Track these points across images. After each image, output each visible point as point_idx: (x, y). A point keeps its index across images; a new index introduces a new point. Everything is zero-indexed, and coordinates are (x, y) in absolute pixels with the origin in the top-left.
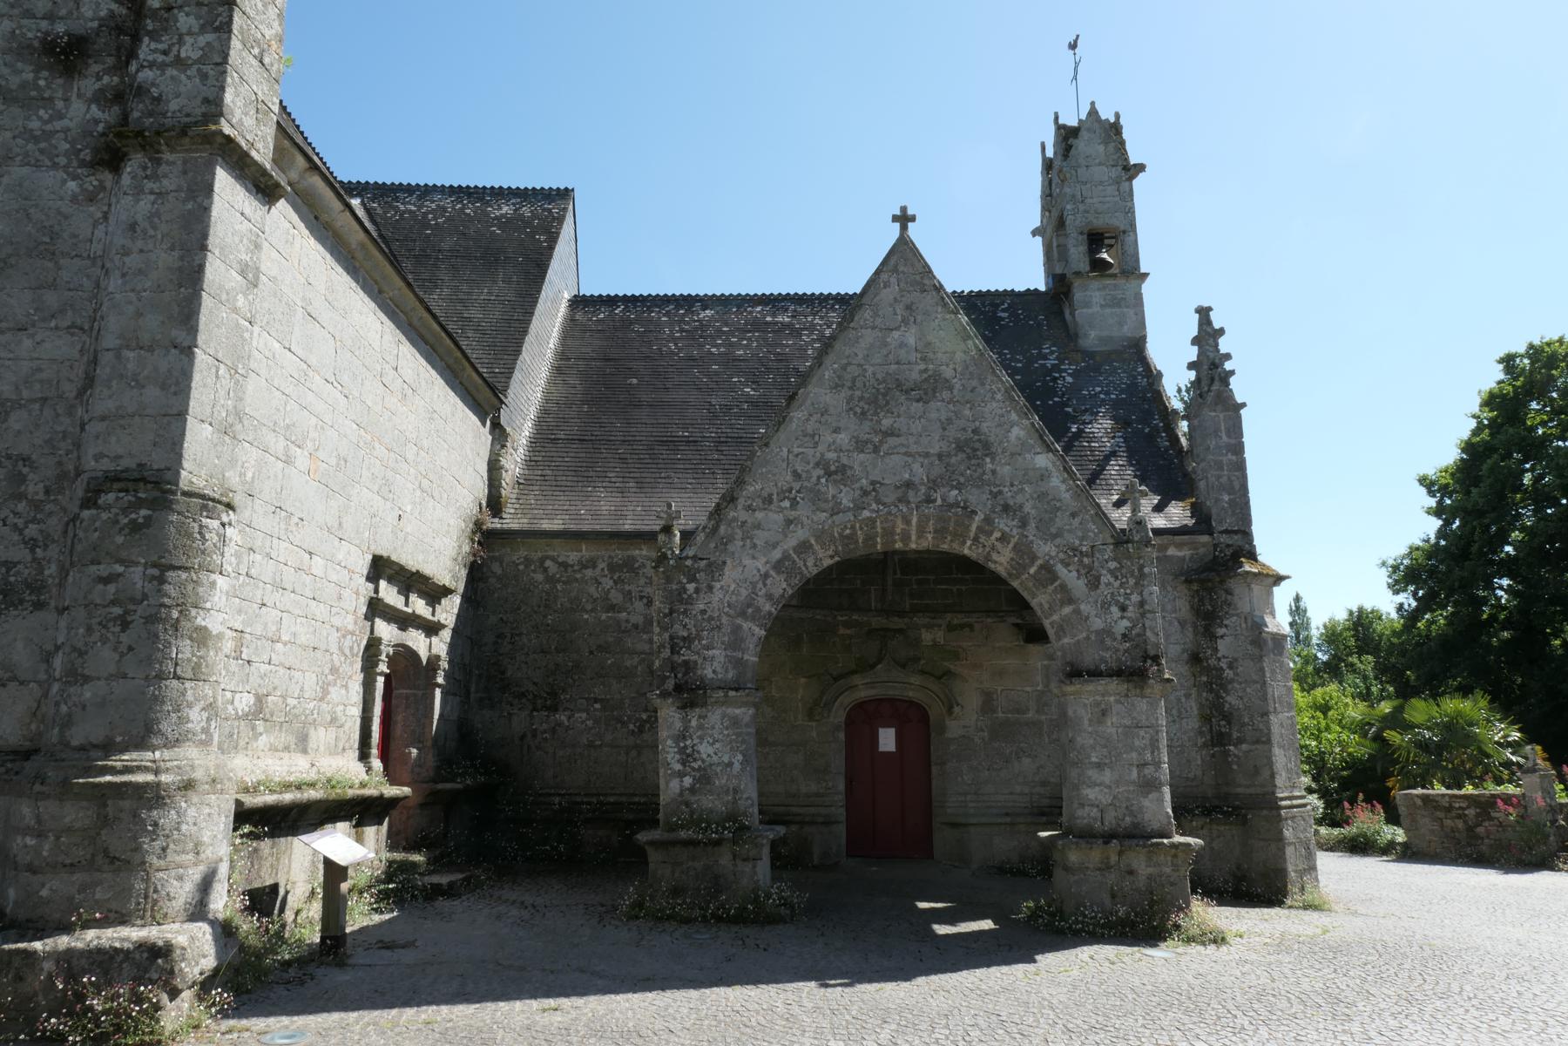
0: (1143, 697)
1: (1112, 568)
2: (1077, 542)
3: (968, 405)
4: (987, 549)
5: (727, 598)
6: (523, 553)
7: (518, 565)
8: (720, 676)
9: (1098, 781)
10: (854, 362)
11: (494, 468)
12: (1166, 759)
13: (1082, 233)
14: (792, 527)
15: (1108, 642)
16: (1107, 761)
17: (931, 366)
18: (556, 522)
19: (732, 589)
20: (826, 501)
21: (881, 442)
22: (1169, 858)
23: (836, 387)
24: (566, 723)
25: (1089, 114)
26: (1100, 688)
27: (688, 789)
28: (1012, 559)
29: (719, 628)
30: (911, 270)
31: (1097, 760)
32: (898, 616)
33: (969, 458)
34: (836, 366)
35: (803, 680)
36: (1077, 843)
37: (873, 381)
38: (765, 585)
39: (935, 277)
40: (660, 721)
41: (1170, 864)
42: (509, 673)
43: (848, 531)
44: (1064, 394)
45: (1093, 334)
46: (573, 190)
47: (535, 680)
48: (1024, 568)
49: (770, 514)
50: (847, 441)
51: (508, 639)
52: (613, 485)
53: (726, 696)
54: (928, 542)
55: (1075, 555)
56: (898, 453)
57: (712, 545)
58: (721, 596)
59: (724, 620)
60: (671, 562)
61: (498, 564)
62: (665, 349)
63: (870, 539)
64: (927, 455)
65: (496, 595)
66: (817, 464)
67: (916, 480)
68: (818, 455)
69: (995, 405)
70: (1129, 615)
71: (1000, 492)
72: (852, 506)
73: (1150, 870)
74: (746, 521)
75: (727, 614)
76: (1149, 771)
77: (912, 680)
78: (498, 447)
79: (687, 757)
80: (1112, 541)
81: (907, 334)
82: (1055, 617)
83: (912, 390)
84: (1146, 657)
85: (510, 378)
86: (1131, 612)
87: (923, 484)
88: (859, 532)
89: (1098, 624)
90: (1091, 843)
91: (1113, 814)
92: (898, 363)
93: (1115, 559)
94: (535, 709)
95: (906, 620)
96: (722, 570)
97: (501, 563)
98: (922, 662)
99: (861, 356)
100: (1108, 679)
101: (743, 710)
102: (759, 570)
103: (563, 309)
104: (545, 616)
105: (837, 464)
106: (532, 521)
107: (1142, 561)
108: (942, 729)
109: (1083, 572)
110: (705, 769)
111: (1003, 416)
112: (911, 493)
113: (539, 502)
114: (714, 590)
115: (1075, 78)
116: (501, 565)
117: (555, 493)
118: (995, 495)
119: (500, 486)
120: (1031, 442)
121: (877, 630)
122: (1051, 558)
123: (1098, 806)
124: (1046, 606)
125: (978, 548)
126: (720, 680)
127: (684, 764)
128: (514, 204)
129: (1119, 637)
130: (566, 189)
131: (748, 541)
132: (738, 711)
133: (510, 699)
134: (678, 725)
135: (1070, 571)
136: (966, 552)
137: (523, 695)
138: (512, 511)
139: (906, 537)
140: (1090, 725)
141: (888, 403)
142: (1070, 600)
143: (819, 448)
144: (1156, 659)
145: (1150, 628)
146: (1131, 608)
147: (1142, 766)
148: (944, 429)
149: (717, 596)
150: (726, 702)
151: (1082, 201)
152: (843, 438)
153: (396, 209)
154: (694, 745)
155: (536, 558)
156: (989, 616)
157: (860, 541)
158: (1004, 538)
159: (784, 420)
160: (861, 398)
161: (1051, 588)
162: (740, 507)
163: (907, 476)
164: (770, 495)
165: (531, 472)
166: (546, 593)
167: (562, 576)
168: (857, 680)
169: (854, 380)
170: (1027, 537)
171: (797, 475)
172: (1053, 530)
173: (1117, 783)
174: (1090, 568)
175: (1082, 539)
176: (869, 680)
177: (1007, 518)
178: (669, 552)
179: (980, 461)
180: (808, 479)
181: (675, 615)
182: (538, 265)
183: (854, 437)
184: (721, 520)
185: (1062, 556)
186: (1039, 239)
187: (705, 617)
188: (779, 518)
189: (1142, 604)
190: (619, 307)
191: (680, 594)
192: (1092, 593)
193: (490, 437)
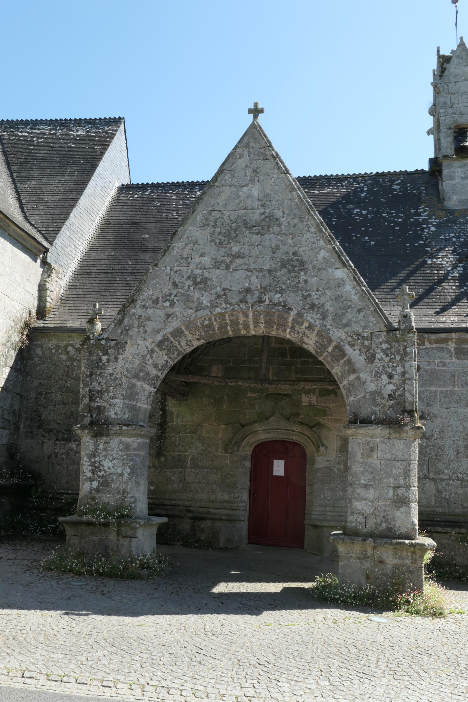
0: (401, 439)
1: (384, 348)
2: (361, 330)
3: (291, 236)
4: (301, 335)
5: (126, 366)
6: (55, 342)
7: (52, 349)
8: (119, 417)
9: (364, 497)
10: (217, 209)
11: (42, 289)
12: (416, 484)
13: (450, 129)
14: (170, 319)
15: (378, 400)
16: (371, 483)
17: (267, 210)
18: (77, 322)
19: (130, 359)
20: (193, 302)
21: (231, 262)
22: (410, 554)
23: (204, 226)
24: (76, 449)
25: (459, 46)
26: (369, 432)
27: (95, 489)
28: (317, 342)
29: (120, 385)
30: (258, 146)
31: (365, 482)
32: (269, 383)
33: (289, 272)
34: (204, 212)
35: (223, 426)
36: (343, 539)
37: (228, 221)
38: (152, 357)
39: (273, 150)
40: (82, 444)
41: (410, 558)
42: (43, 417)
43: (207, 322)
44: (427, 239)
45: (455, 198)
46: (124, 118)
47: (59, 421)
48: (325, 348)
49: (157, 310)
50: (209, 262)
51: (43, 396)
52: (118, 300)
53: (121, 429)
54: (261, 330)
55: (359, 339)
56: (242, 270)
57: (119, 331)
58: (123, 364)
59: (124, 380)
60: (92, 342)
61: (40, 349)
62: (170, 216)
63: (223, 327)
64: (261, 270)
65: (38, 368)
66: (189, 278)
67: (253, 287)
68: (190, 271)
69: (309, 235)
70: (395, 381)
71: (309, 295)
72: (209, 305)
73: (395, 561)
74: (141, 316)
75: (126, 376)
76: (401, 491)
77: (294, 429)
78: (46, 276)
79: (95, 468)
80: (384, 329)
81: (254, 188)
82: (345, 382)
83: (254, 227)
84: (404, 411)
85: (57, 234)
86: (396, 380)
87: (257, 290)
88: (215, 323)
89: (372, 387)
90: (353, 540)
91: (374, 520)
92: (245, 209)
93: (387, 342)
94: (57, 440)
95: (274, 386)
96: (125, 347)
97: (42, 348)
98: (302, 416)
99: (221, 204)
100: (375, 426)
101: (132, 439)
102: (147, 348)
103: (112, 193)
104: (66, 382)
105: (201, 277)
106: (62, 322)
107: (405, 344)
108: (313, 462)
109: (364, 350)
110: (106, 477)
111: (314, 243)
112: (249, 296)
113: (70, 311)
114: (119, 360)
115: (456, 23)
116: (42, 350)
117: (82, 305)
118: (305, 298)
119: (46, 301)
120: (333, 260)
121: (271, 394)
122: (342, 340)
123: (363, 514)
124: (340, 374)
125: (294, 334)
126: (120, 419)
127: (93, 473)
128: (86, 129)
129: (386, 397)
130: (120, 118)
131: (142, 328)
132: (129, 440)
133: (43, 433)
134: (92, 447)
135: (354, 350)
136: (288, 336)
137: (51, 431)
138: (53, 316)
139: (246, 327)
140: (362, 458)
141: (237, 236)
142: (353, 371)
143: (190, 267)
144: (411, 413)
145: (408, 391)
146: (396, 377)
147: (396, 488)
148: (274, 253)
149: (121, 363)
150: (121, 434)
151: (451, 107)
152: (206, 260)
153: (16, 135)
154: (101, 461)
155: (62, 345)
156: (329, 385)
157: (216, 329)
158: (311, 327)
159: (168, 249)
160: (220, 233)
161: (342, 361)
162: (138, 306)
163: (247, 285)
164: (157, 298)
165: (70, 293)
166: (68, 367)
167: (77, 357)
168: (257, 427)
169: (216, 222)
170: (326, 326)
171: (175, 285)
172: (344, 321)
173: (378, 499)
174: (369, 348)
175: (364, 328)
176: (266, 428)
177: (313, 313)
178: (91, 336)
179: (297, 274)
180: (182, 287)
181: (94, 376)
182: (92, 165)
183: (213, 259)
184: (125, 315)
185: (349, 339)
186: (432, 137)
187: (113, 378)
188: (162, 313)
189: (404, 374)
190: (148, 190)
191: (97, 363)
192: (369, 366)
193: (41, 270)
